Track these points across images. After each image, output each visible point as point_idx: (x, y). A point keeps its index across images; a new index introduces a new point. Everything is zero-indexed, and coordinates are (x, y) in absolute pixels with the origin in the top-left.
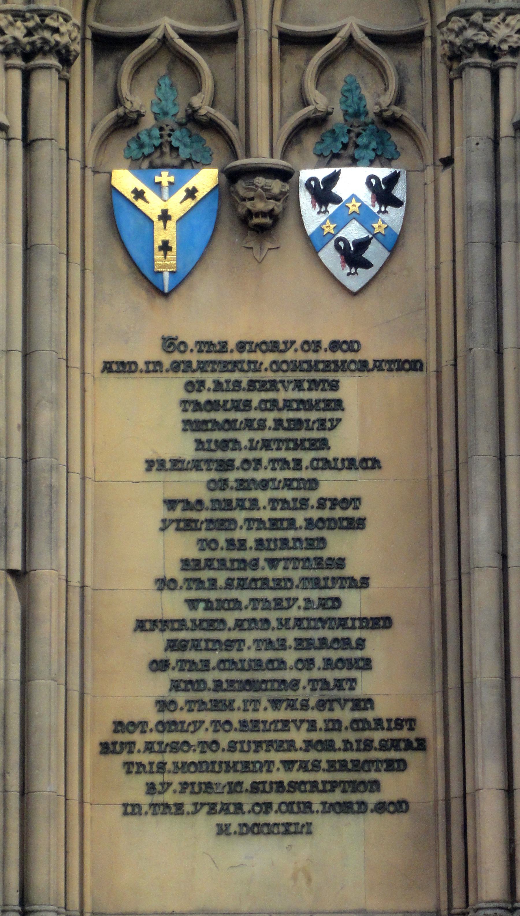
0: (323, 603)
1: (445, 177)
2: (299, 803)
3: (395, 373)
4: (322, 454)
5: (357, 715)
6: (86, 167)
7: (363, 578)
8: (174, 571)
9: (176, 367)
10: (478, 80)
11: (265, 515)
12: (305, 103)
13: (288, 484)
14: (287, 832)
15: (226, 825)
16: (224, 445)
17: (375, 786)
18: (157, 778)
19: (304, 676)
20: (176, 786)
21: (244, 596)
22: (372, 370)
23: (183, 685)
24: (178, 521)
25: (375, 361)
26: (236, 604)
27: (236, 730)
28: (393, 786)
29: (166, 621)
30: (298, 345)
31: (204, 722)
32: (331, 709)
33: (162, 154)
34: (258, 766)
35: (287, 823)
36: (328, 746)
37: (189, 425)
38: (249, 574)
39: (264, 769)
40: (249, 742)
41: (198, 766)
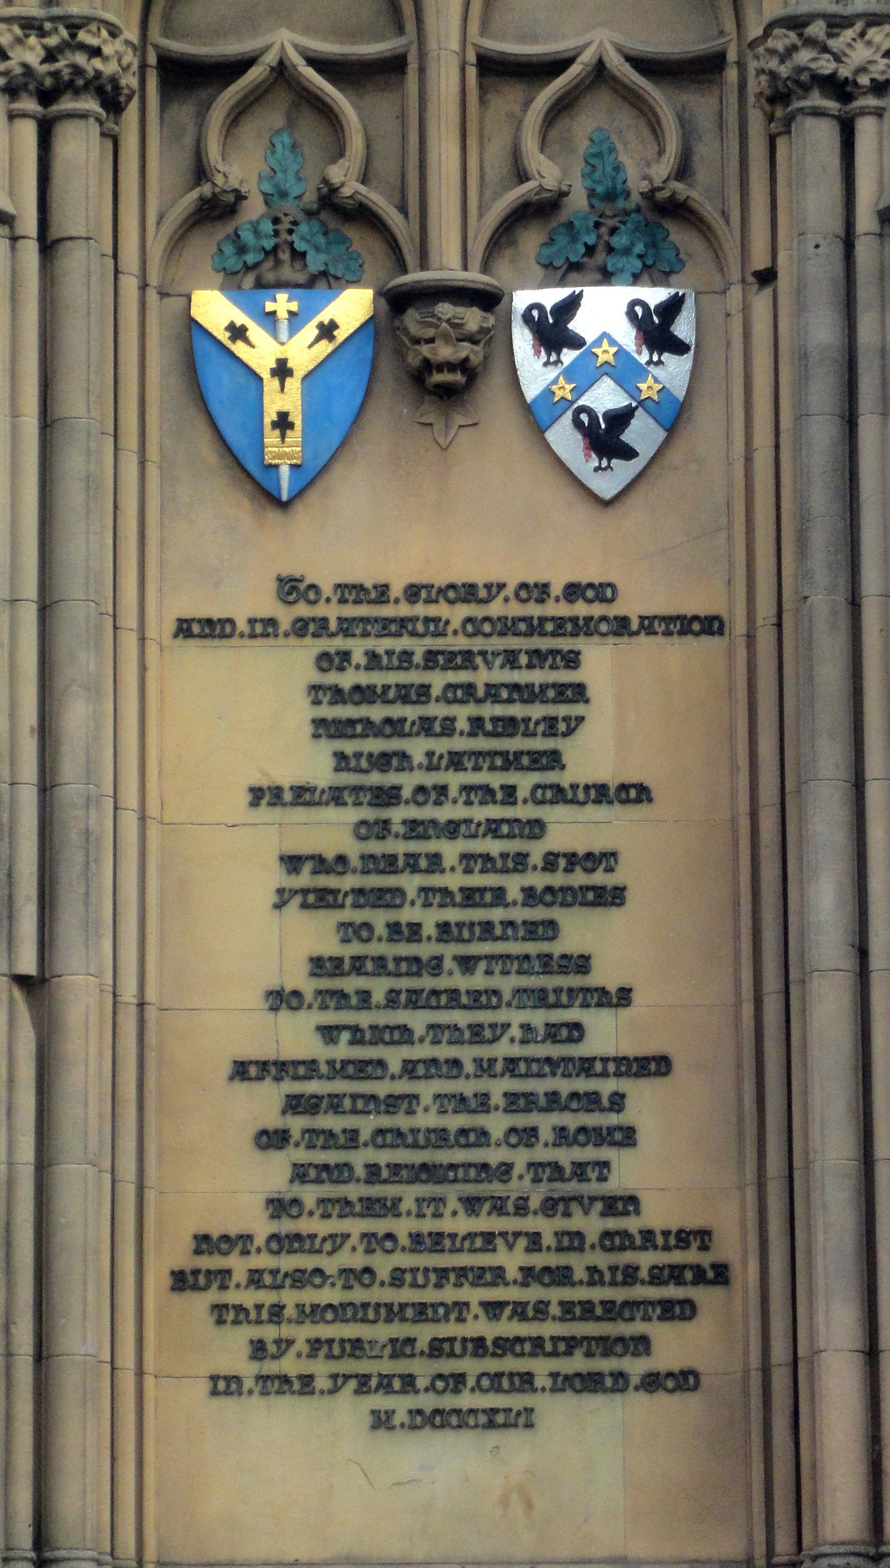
0: (553, 1033)
1: (761, 303)
2: (511, 1375)
3: (675, 639)
4: (551, 777)
5: (612, 1224)
6: (147, 285)
7: (622, 990)
8: (297, 978)
9: (301, 628)
10: (818, 138)
11: (454, 881)
12: (522, 176)
13: (493, 828)
14: (491, 1425)
15: (386, 1412)
16: (383, 761)
17: (641, 1345)
18: (269, 1332)
19: (520, 1158)
20: (301, 1345)
21: (418, 1021)
22: (637, 633)
23: (312, 1173)
24: (305, 892)
25: (642, 618)
26: (405, 1034)
27: (403, 1249)
28: (672, 1346)
29: (284, 1064)
30: (509, 591)
31: (348, 1236)
32: (567, 1214)
33: (278, 263)
34: (441, 1311)
35: (492, 1409)
36: (561, 1276)
37: (323, 728)
38: (427, 982)
39: (453, 1317)
40: (426, 1270)
41: (339, 1312)
